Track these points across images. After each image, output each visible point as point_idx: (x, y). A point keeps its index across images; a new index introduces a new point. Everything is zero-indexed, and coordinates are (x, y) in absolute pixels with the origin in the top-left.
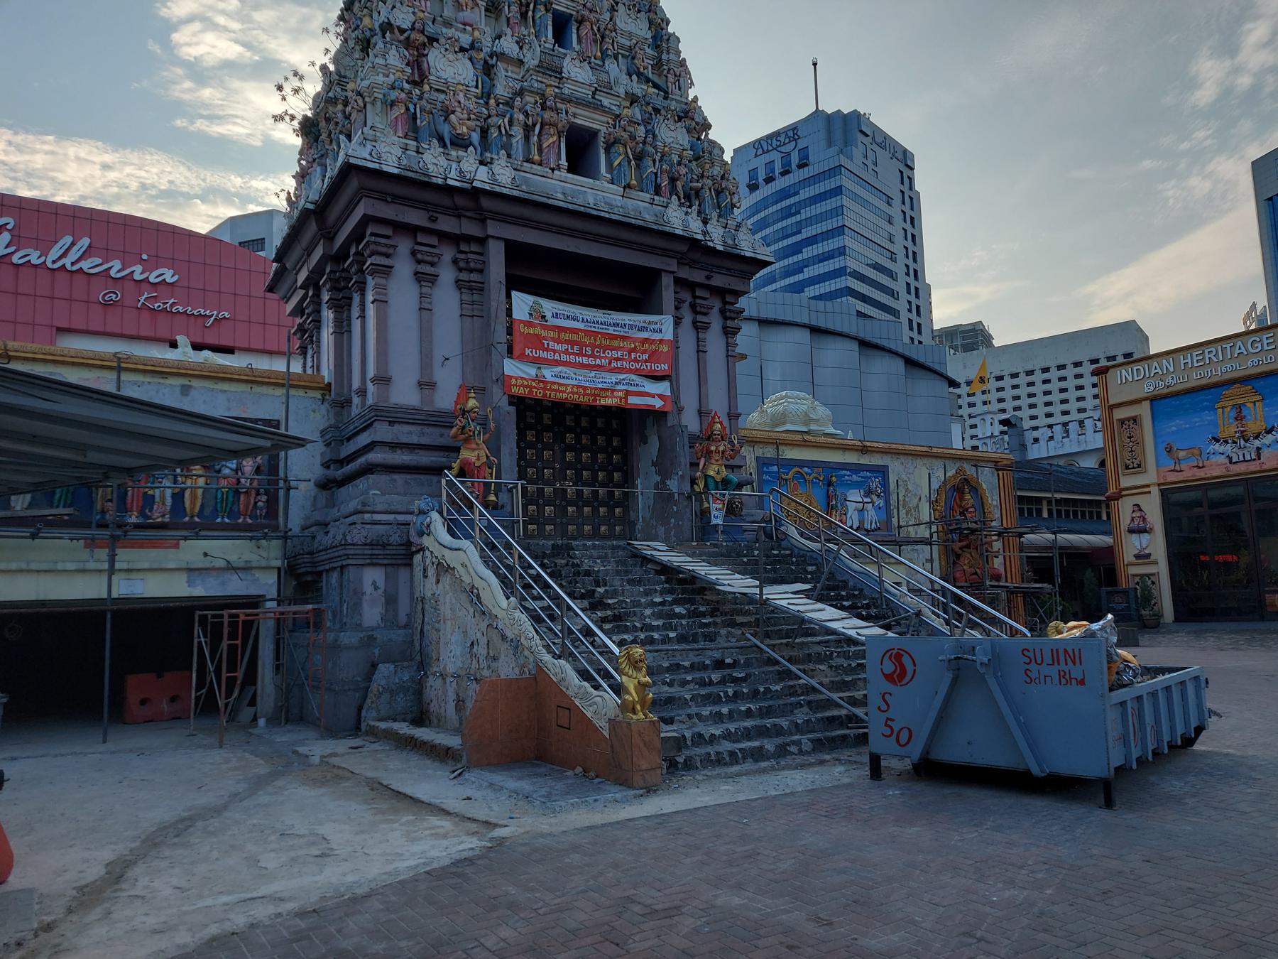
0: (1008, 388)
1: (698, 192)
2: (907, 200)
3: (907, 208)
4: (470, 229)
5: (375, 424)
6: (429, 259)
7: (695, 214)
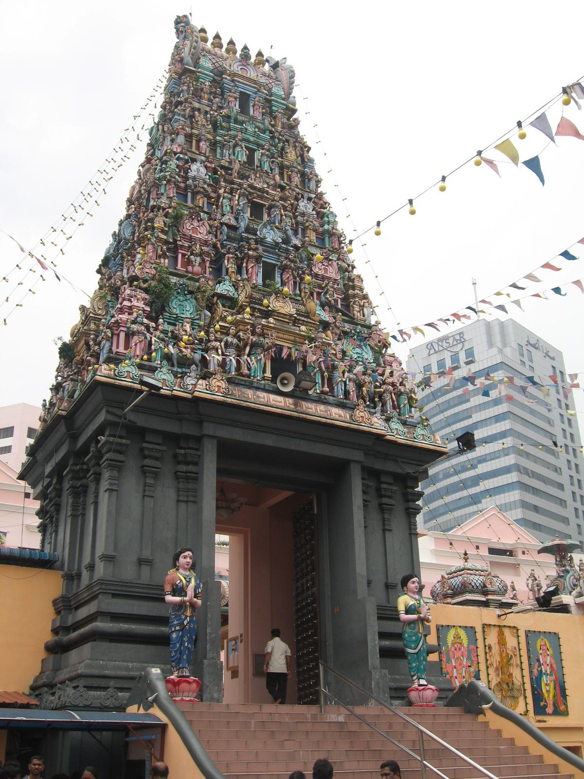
1: (381, 396)
2: (561, 390)
3: (561, 397)
4: (188, 429)
5: (100, 596)
6: (156, 455)
7: (378, 415)
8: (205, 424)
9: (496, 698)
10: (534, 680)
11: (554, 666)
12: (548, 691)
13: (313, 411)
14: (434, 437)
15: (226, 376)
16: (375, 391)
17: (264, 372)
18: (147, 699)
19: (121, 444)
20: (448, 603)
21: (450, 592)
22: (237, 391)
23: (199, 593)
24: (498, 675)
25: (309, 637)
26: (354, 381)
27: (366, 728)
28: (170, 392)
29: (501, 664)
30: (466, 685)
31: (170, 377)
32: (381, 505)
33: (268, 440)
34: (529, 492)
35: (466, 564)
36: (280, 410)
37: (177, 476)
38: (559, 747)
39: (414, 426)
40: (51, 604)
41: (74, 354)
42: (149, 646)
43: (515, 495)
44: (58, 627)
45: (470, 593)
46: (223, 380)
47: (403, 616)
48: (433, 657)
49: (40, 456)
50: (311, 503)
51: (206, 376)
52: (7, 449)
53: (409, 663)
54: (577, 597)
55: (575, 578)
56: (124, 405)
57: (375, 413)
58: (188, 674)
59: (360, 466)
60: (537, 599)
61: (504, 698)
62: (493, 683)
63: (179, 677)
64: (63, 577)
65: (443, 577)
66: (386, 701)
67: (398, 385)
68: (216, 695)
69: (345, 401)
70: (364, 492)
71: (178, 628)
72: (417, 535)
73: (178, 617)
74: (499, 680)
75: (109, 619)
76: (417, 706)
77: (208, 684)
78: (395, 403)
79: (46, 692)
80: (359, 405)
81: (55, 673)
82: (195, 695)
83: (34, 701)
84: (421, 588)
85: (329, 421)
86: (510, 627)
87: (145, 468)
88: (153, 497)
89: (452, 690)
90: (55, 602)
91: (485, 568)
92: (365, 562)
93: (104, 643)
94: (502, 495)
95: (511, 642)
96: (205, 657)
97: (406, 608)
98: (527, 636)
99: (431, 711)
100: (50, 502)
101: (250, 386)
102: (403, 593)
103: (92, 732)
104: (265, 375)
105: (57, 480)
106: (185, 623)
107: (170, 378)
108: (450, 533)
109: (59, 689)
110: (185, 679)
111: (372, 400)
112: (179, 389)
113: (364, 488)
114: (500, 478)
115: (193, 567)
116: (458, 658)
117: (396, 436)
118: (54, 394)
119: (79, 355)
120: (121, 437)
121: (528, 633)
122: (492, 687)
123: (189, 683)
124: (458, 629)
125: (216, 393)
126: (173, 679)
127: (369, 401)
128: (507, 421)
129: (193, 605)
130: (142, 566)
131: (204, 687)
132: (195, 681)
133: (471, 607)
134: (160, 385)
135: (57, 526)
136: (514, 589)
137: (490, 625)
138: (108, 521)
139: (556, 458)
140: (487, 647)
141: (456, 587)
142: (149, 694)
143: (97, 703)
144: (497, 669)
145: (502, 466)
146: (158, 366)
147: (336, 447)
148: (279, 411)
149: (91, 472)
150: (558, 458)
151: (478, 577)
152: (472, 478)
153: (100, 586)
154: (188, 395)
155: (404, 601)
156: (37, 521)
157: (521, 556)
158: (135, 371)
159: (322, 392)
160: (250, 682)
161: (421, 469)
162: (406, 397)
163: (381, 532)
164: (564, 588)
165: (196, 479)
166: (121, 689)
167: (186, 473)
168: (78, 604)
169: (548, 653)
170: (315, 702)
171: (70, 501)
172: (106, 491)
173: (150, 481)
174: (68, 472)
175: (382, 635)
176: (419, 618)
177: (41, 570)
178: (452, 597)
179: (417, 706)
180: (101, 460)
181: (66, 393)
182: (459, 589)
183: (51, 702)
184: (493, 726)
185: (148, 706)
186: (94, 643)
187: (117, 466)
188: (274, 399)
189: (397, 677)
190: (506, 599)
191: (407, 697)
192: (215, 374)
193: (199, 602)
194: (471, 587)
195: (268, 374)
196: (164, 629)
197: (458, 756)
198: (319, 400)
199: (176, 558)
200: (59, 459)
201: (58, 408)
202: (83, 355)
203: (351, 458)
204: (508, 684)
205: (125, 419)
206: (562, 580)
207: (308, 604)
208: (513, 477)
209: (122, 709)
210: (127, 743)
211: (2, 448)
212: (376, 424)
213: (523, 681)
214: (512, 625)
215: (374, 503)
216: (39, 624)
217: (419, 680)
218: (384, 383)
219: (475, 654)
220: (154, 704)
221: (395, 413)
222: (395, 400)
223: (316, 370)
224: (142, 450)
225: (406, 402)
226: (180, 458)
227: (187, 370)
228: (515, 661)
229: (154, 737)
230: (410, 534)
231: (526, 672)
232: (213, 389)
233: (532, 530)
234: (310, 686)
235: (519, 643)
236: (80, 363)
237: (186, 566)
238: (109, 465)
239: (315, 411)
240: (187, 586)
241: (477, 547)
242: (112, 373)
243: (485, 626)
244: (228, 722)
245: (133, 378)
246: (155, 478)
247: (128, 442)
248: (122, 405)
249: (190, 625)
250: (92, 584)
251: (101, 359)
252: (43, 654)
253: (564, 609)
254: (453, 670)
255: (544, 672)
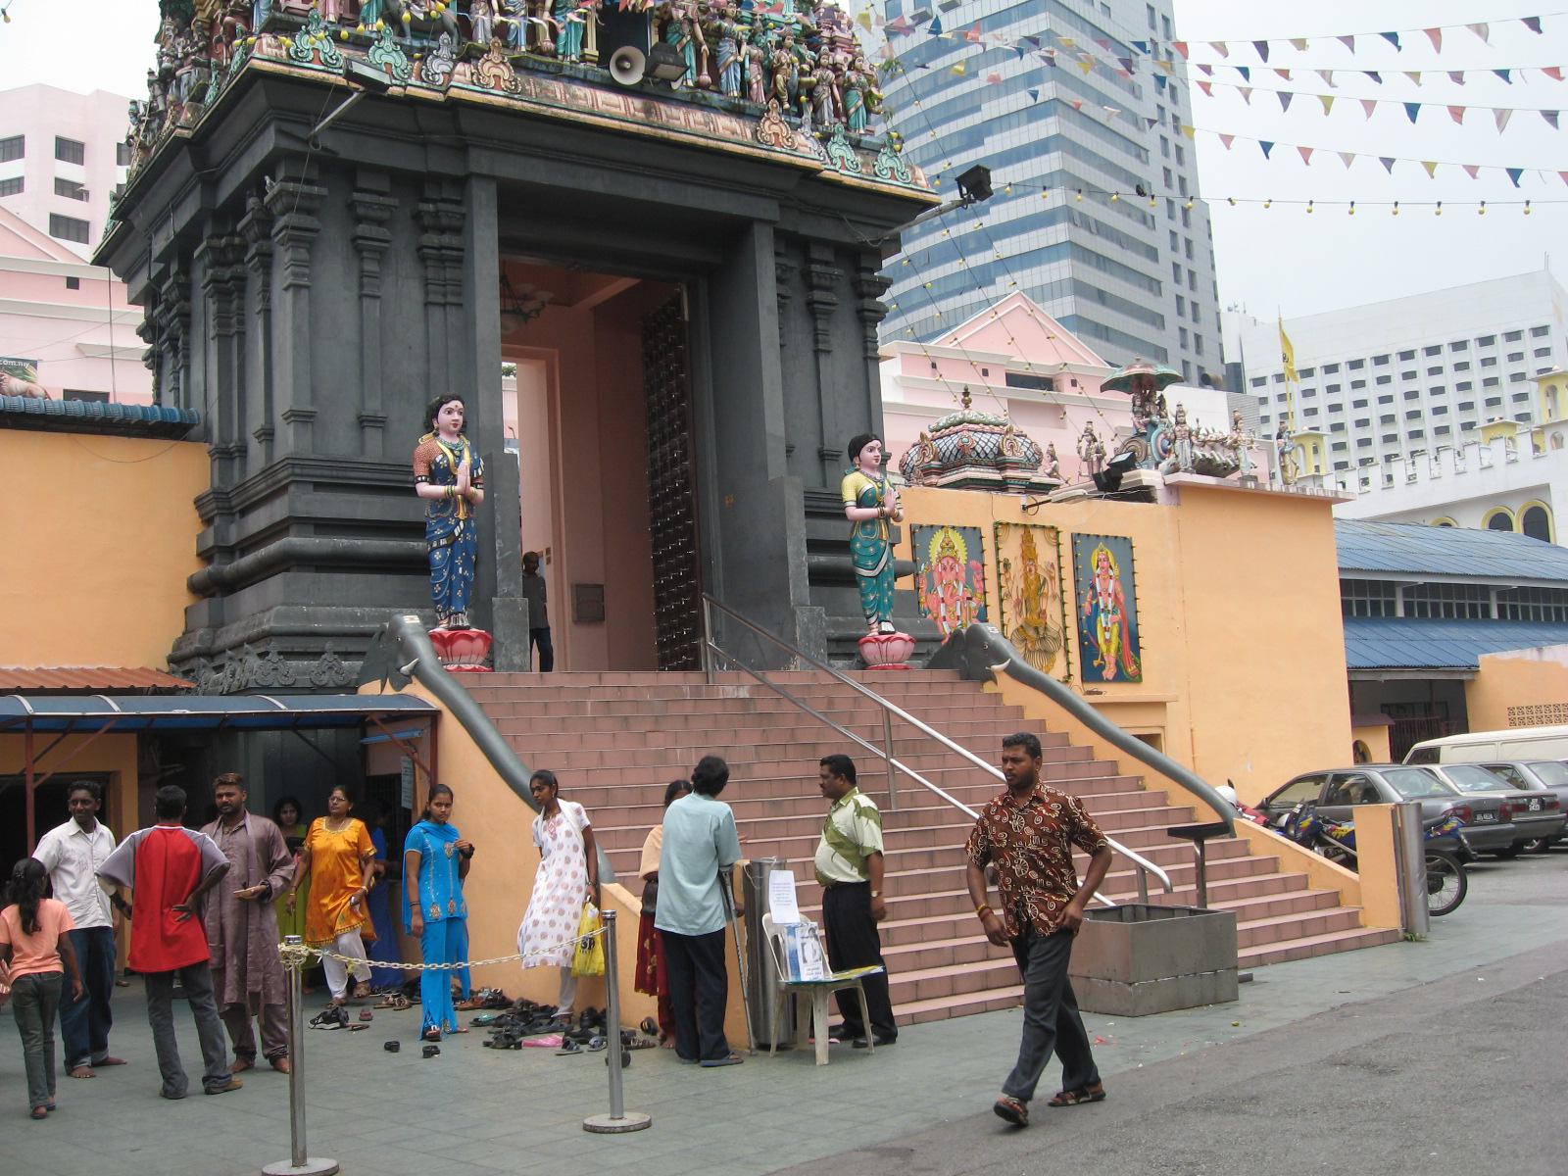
0: (1448, 369)
1: (811, 91)
4: (440, 163)
5: (292, 489)
6: (379, 214)
7: (807, 129)
8: (474, 153)
9: (1015, 654)
10: (1084, 621)
11: (1121, 596)
12: (1108, 641)
13: (681, 123)
14: (914, 173)
15: (509, 55)
16: (800, 82)
17: (584, 44)
18: (399, 670)
19: (310, 196)
20: (931, 485)
21: (935, 463)
22: (532, 85)
23: (478, 477)
24: (1020, 613)
25: (677, 550)
26: (761, 62)
27: (787, 707)
28: (400, 90)
29: (1026, 595)
30: (964, 631)
31: (399, 60)
32: (810, 304)
33: (597, 183)
34: (1090, 264)
35: (967, 411)
36: (617, 122)
37: (422, 256)
38: (1127, 735)
39: (875, 151)
40: (193, 507)
41: (193, 7)
42: (388, 576)
43: (1062, 270)
44: (212, 548)
45: (973, 465)
46: (503, 63)
47: (853, 511)
48: (904, 584)
49: (140, 219)
50: (677, 302)
51: (469, 55)
52: (15, 185)
53: (863, 595)
54: (1169, 473)
55: (1166, 437)
56: (312, 118)
57: (801, 126)
58: (466, 624)
59: (772, 231)
60: (1096, 477)
61: (1028, 654)
62: (1012, 627)
63: (450, 629)
64: (211, 454)
65: (923, 436)
66: (823, 661)
67: (845, 69)
68: (517, 660)
69: (742, 102)
70: (780, 280)
71: (443, 542)
72: (877, 359)
73: (442, 522)
74: (1020, 622)
75: (312, 528)
76: (876, 668)
77: (502, 640)
78: (840, 105)
79: (204, 666)
80: (768, 111)
81: (215, 632)
82: (481, 659)
83: (185, 684)
84: (885, 458)
85: (712, 143)
86: (1044, 527)
87: (360, 242)
88: (378, 297)
89: (939, 640)
90: (199, 503)
91: (1002, 420)
92: (781, 411)
93: (307, 574)
94: (1036, 270)
95: (1045, 554)
96: (495, 593)
97: (857, 496)
98: (1074, 544)
99: (902, 677)
100: (168, 309)
101: (557, 74)
102: (852, 469)
103: (303, 732)
104: (586, 51)
105: (179, 265)
106: (457, 532)
107: (399, 61)
108: (933, 343)
109: (231, 658)
110: (461, 632)
111: (794, 100)
112: (419, 83)
113: (779, 271)
114: (1033, 234)
115: (463, 430)
116: (949, 584)
117: (841, 171)
118: (158, 92)
119: (204, 11)
120: (309, 182)
121: (1076, 538)
122: (1009, 635)
123: (470, 639)
124: (950, 531)
125: (492, 91)
126: (440, 634)
127: (789, 101)
128: (1052, 119)
129: (468, 500)
130: (366, 429)
131: (496, 645)
132: (480, 635)
133: (975, 492)
134: (386, 80)
135: (187, 357)
136: (1053, 458)
137: (1008, 524)
138: (295, 347)
139: (1142, 162)
140: (1001, 564)
141: (947, 454)
142: (401, 661)
143: (304, 681)
144: (1018, 603)
145: (1023, 143)
146: (374, 36)
147: (726, 194)
148: (615, 124)
149: (252, 251)
150: (1146, 162)
151: (988, 436)
152: (975, 235)
153: (290, 471)
154: (437, 94)
155: (853, 483)
156: (143, 346)
157: (1068, 390)
158: (328, 48)
159: (698, 85)
160: (568, 635)
161: (887, 235)
162: (860, 94)
163: (810, 355)
164: (1146, 455)
165: (459, 261)
166: (346, 655)
167: (440, 248)
168: (247, 503)
169: (1111, 573)
170: (693, 665)
171: (212, 308)
172: (286, 289)
173: (371, 267)
174: (204, 251)
175: (814, 546)
176: (882, 513)
177: (173, 442)
178: (939, 474)
179: (876, 668)
180: (272, 227)
181: (184, 90)
182: (952, 458)
183: (217, 683)
184: (1008, 701)
185: (402, 681)
186: (289, 575)
187: (305, 240)
188: (605, 100)
189: (840, 619)
190: (1039, 477)
191: (860, 654)
192: (489, 51)
193: (480, 493)
194: (974, 455)
195: (592, 50)
196: (415, 544)
197: (952, 749)
198: (693, 102)
199: (433, 413)
200: (183, 224)
201: (173, 123)
202: (213, 11)
203: (754, 215)
204: (1036, 629)
205: (316, 146)
206: (1143, 441)
207: (675, 491)
208: (1059, 233)
209: (351, 689)
210: (365, 747)
211: (3, 182)
212: (802, 147)
213: (1064, 623)
214: (1047, 524)
215: (798, 301)
216: (173, 546)
217: (880, 623)
218: (818, 65)
219: (979, 578)
220: (413, 677)
221: (840, 127)
222: (838, 98)
223: (685, 41)
224: (351, 206)
225: (860, 102)
226: (427, 221)
227: (433, 44)
228: (1052, 588)
229: (416, 734)
230: (866, 359)
231: (1070, 609)
232: (485, 82)
233: (1093, 340)
234: (682, 639)
235: (1059, 557)
236: (207, 26)
237: (452, 428)
238: (291, 239)
239: (686, 123)
240: (457, 465)
241: (985, 373)
242: (284, 53)
243: (998, 526)
244: (546, 704)
245: (326, 63)
246: (380, 262)
247: (324, 191)
248: (308, 118)
249: (465, 536)
250: (273, 466)
251: (258, 22)
252: (185, 599)
253: (1144, 494)
254: (939, 606)
255: (1102, 607)
